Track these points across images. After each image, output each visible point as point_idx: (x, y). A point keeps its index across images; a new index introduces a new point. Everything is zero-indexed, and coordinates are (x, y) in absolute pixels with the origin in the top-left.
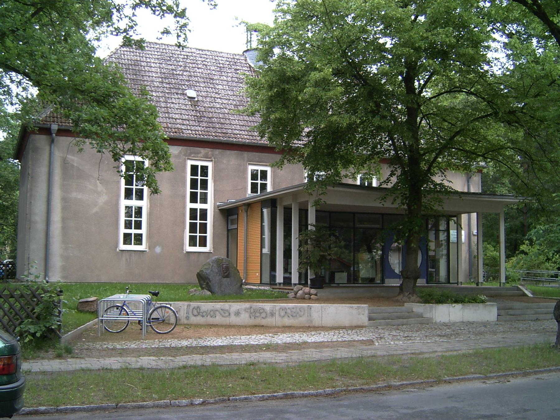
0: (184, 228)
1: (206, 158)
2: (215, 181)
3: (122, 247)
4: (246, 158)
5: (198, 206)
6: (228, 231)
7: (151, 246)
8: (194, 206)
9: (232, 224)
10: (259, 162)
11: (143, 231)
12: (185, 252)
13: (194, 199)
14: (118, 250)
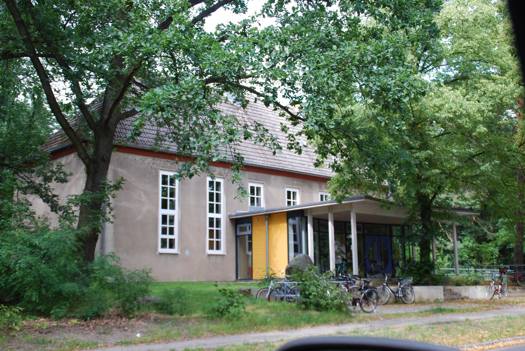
0: (206, 234)
1: (220, 175)
2: (227, 194)
3: (161, 250)
4: (247, 177)
5: (214, 215)
6: (237, 237)
7: (182, 250)
8: (164, 236)
9: (241, 231)
10: (256, 180)
11: (175, 236)
12: (206, 255)
13: (164, 231)
14: (157, 253)
